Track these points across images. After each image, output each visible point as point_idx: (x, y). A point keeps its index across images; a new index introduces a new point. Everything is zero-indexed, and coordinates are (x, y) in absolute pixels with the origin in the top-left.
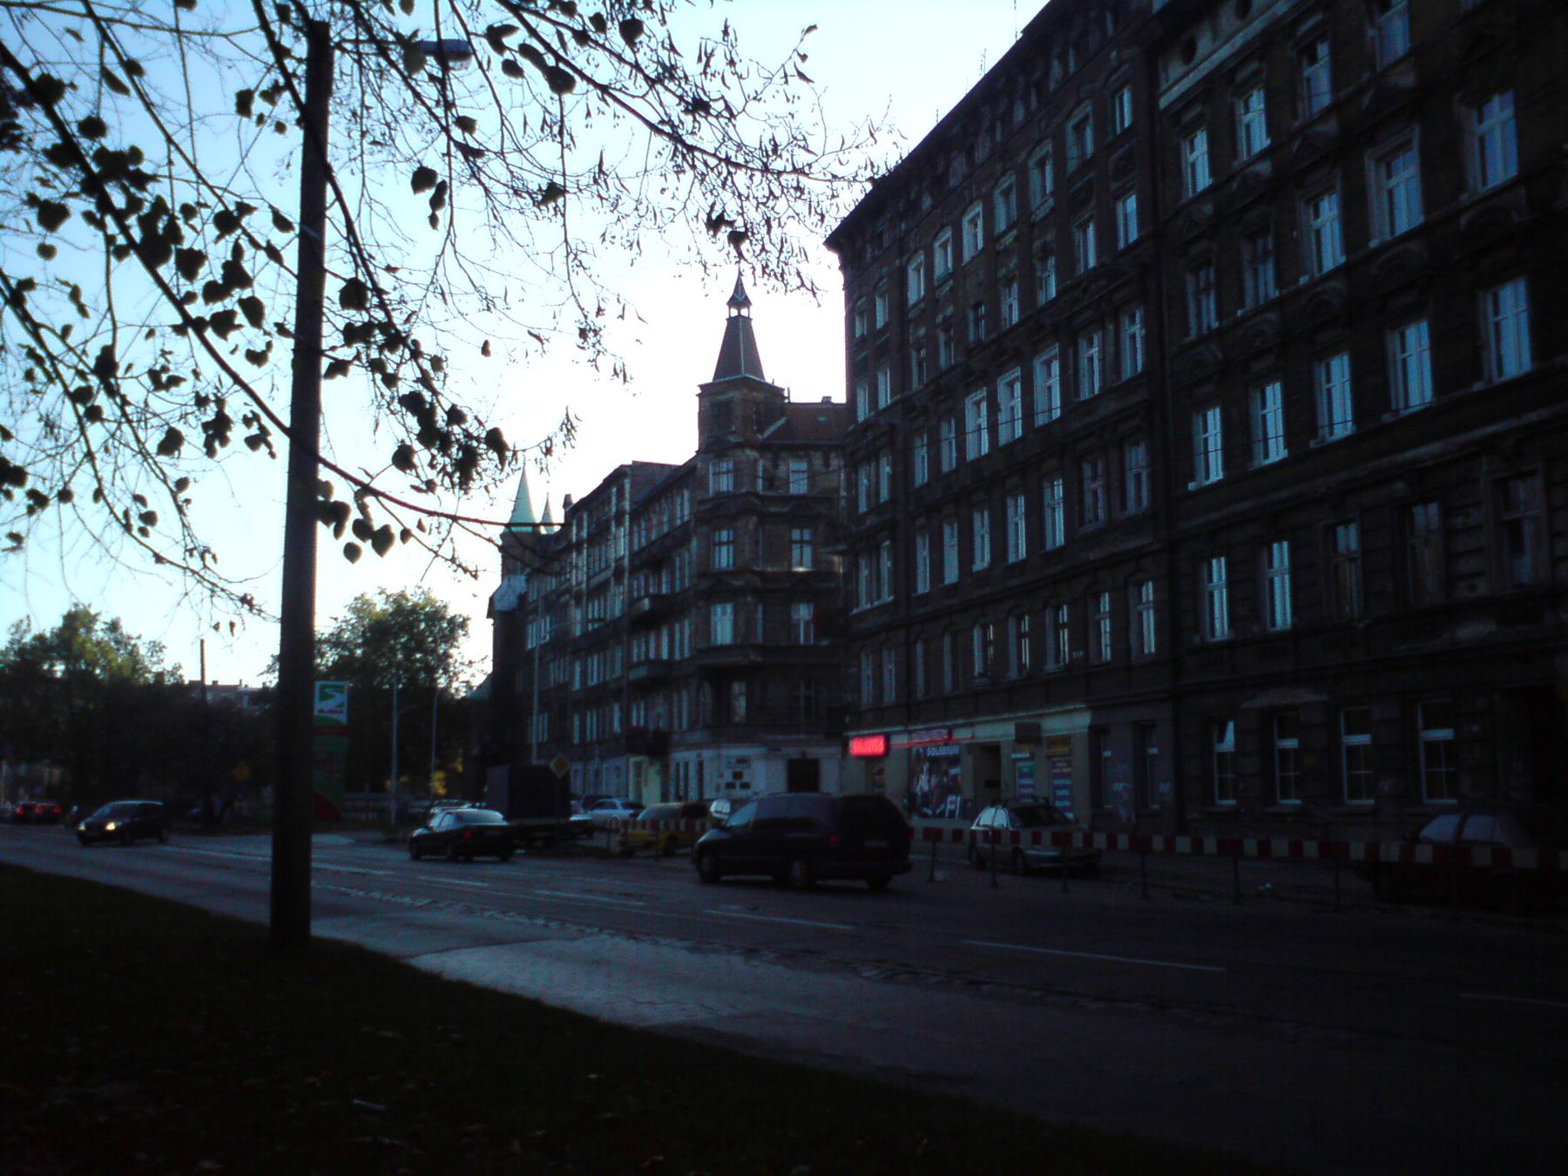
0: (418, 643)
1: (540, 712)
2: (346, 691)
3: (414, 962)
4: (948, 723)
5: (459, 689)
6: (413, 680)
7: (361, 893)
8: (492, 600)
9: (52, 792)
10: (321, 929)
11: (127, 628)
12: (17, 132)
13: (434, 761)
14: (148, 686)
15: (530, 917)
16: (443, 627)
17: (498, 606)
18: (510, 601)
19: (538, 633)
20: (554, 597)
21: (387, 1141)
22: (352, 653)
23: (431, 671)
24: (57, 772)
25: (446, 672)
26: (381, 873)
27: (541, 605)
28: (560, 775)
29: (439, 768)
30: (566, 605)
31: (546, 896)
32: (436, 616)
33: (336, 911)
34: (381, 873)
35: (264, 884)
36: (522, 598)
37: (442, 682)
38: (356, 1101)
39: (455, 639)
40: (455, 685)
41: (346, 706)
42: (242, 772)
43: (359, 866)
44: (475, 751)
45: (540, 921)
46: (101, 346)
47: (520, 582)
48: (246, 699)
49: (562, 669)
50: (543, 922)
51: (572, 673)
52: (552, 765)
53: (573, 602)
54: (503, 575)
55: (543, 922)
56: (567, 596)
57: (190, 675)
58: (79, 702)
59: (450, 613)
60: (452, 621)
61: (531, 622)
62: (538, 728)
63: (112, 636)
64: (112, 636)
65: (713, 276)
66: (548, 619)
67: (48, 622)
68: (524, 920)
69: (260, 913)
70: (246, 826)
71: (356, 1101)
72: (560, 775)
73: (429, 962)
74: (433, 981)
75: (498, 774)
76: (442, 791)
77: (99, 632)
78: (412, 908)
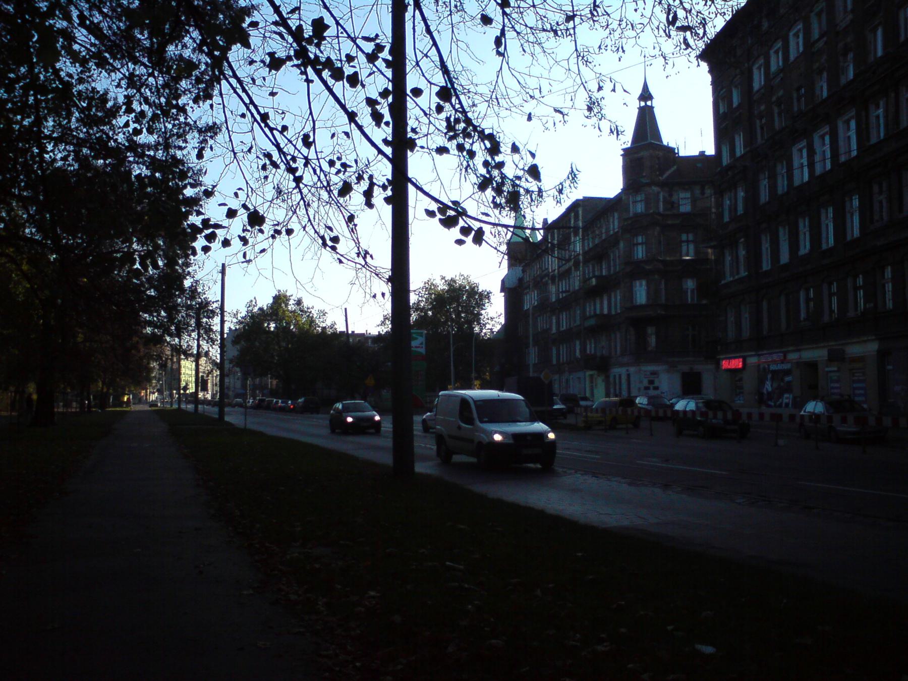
2: (424, 336)
8: (503, 282)
13: (473, 375)
17: (507, 285)
19: (530, 300)
21: (466, 586)
23: (470, 323)
25: (479, 324)
28: (547, 382)
29: (476, 379)
30: (546, 284)
36: (520, 280)
38: (448, 563)
44: (497, 369)
47: (519, 270)
52: (542, 376)
53: (550, 282)
58: (284, 344)
60: (481, 295)
61: (526, 294)
62: (533, 356)
67: (265, 301)
71: (448, 563)
77: (292, 307)
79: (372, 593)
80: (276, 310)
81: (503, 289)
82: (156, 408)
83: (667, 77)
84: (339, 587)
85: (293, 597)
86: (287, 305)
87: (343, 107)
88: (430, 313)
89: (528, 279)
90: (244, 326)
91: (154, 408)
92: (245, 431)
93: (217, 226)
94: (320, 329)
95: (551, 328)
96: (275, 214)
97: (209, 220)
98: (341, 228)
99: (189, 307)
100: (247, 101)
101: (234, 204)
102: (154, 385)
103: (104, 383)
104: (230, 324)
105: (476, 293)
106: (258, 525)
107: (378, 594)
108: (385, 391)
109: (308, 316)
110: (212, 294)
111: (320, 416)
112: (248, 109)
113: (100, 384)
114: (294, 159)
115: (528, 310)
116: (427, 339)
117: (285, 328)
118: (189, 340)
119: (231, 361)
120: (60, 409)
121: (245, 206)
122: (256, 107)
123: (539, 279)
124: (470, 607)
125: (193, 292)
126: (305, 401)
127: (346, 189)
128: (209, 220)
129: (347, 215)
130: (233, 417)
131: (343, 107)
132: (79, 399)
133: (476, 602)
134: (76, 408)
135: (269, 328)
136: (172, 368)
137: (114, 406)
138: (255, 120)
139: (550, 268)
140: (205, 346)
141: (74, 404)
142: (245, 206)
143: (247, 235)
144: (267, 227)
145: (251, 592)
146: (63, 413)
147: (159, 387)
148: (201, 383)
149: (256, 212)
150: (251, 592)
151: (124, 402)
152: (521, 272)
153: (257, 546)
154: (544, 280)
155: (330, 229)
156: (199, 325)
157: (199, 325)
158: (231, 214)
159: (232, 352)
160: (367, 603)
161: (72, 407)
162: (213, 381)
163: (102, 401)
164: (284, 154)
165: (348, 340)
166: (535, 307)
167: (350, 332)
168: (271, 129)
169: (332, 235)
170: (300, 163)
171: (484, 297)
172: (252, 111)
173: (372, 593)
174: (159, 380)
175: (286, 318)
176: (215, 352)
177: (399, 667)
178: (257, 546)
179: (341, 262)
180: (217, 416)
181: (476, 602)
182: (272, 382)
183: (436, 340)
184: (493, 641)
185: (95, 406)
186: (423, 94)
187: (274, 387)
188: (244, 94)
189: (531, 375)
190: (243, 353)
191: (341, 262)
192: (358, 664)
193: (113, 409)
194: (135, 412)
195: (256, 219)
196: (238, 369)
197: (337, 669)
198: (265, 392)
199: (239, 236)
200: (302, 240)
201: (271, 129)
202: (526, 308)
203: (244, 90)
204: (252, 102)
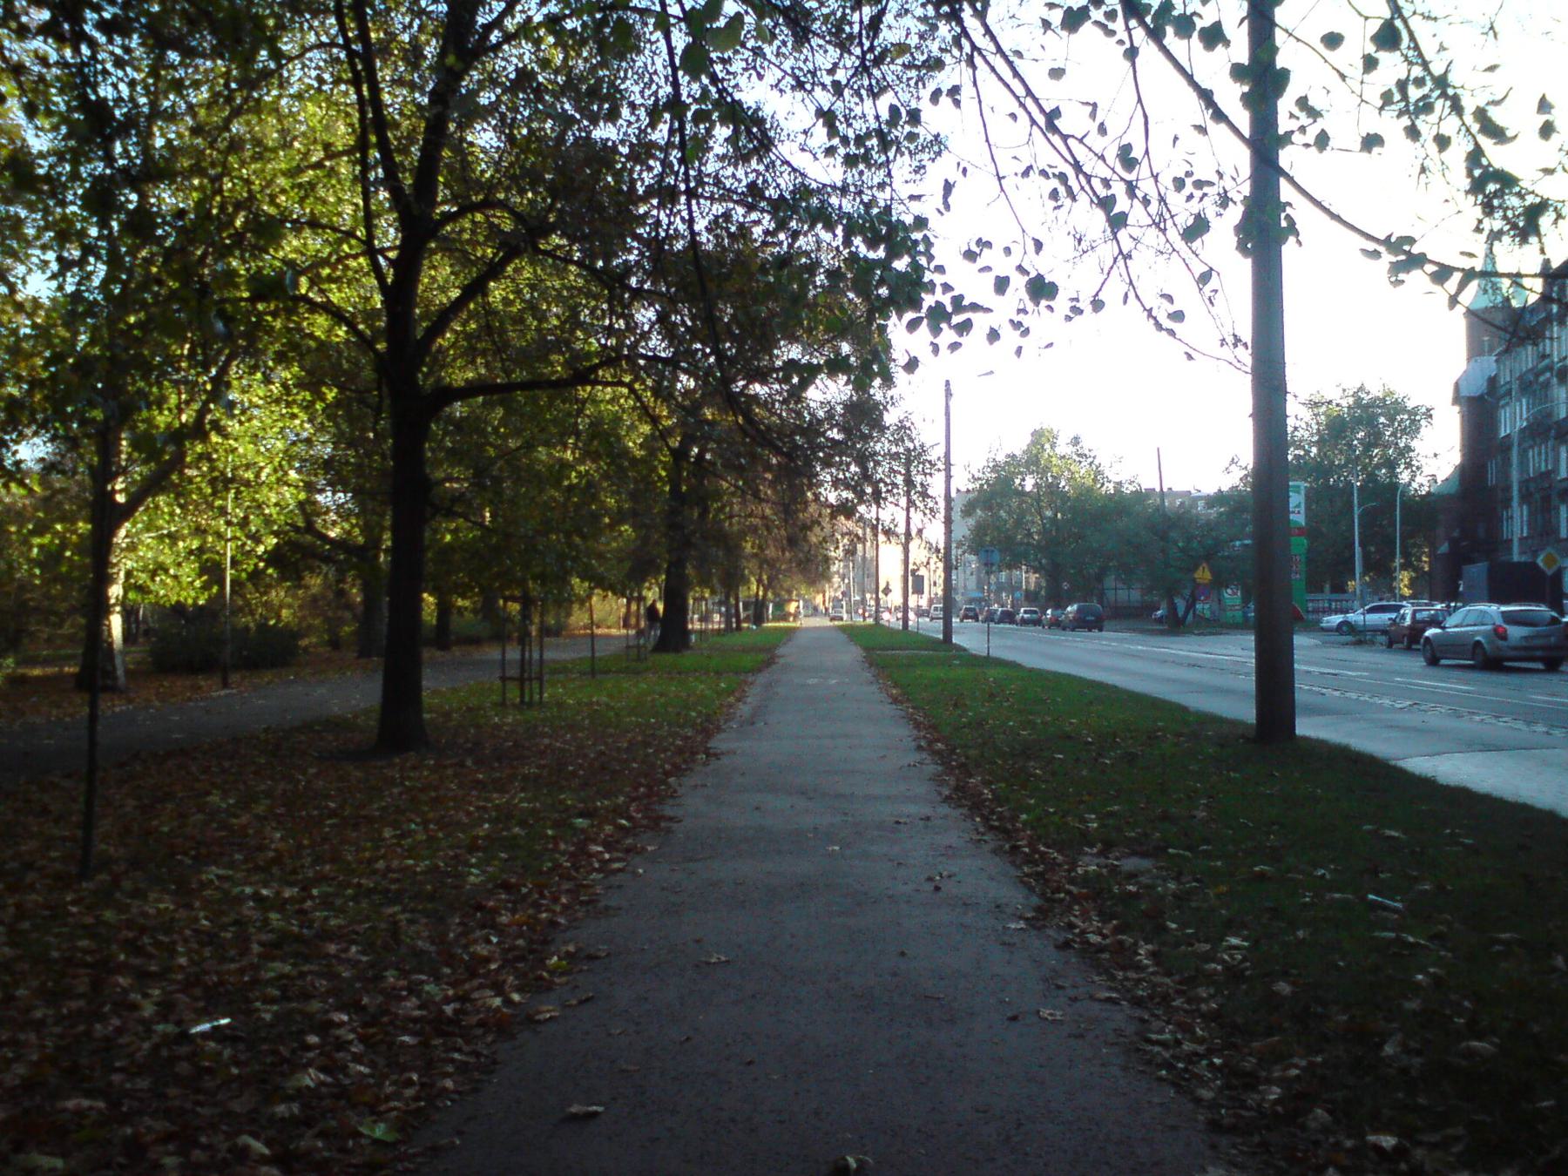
0: (1375, 439)
1: (1521, 505)
2: (1303, 492)
3: (1401, 764)
4: (309, 538)
5: (1421, 484)
6: (1372, 477)
7: (1337, 694)
8: (1457, 386)
9: (1031, 597)
10: (1305, 727)
11: (1086, 444)
12: (610, 144)
13: (1398, 561)
14: (1110, 497)
15: (1529, 723)
16: (1414, 420)
17: (1465, 393)
18: (1478, 387)
19: (1513, 419)
20: (1531, 378)
21: (1411, 939)
22: (1308, 452)
23: (1391, 465)
24: (1033, 577)
25: (1409, 465)
26: (1354, 674)
27: (1515, 386)
28: (1549, 573)
29: (1404, 567)
30: (1547, 385)
31: (1544, 702)
32: (1393, 408)
33: (1315, 711)
34: (1354, 674)
35: (1249, 683)
36: (1492, 381)
37: (1404, 477)
38: (1371, 897)
39: (1418, 430)
40: (1419, 479)
41: (1303, 506)
42: (1204, 575)
43: (1328, 666)
44: (1444, 548)
45: (1540, 728)
46: (1231, 81)
47: (1489, 364)
48: (1201, 504)
49: (1543, 457)
50: (1544, 729)
51: (1557, 461)
52: (1540, 561)
53: (1555, 380)
54: (1469, 360)
55: (1544, 729)
56: (1548, 375)
57: (1149, 482)
58: (1049, 513)
59: (1410, 405)
60: (1413, 412)
61: (1503, 407)
62: (1517, 522)
63: (1074, 449)
64: (1074, 449)
65: (1487, 17)
66: (1524, 401)
67: (1018, 444)
68: (1520, 725)
69: (1247, 712)
70: (1216, 626)
71: (1371, 897)
72: (1549, 573)
73: (1419, 765)
74: (1427, 787)
75: (1476, 571)
76: (1407, 592)
77: (1063, 448)
78: (1393, 710)
79: (1234, 941)
80: (1036, 456)
81: (1457, 399)
82: (841, 623)
83: (1492, 68)
84: (1174, 926)
85: (1094, 938)
86: (1053, 446)
87: (1190, 79)
88: (1314, 450)
89: (1508, 379)
90: (982, 485)
91: (837, 623)
92: (988, 661)
93: (975, 307)
94: (1111, 486)
95: (1556, 470)
96: (1075, 280)
97: (961, 297)
98: (1188, 297)
99: (895, 457)
100: (1021, 91)
101: (1005, 267)
102: (836, 585)
103: (759, 581)
104: (962, 482)
105: (1404, 410)
106: (1024, 817)
107: (1246, 944)
108: (1229, 591)
109: (1091, 464)
110: (928, 435)
111: (1104, 634)
112: (1022, 105)
113: (754, 587)
114: (1106, 183)
115: (1508, 436)
116: (1307, 497)
117: (1049, 486)
118: (891, 513)
119: (960, 544)
120: (695, 625)
121: (1020, 268)
122: (1036, 100)
123: (1531, 378)
124: (1420, 977)
125: (902, 428)
126: (1079, 610)
127: (1198, 228)
128: (961, 297)
129: (1199, 269)
130: (969, 637)
131: (1190, 79)
132: (723, 609)
133: (1432, 970)
134: (720, 623)
135: (1023, 486)
136: (864, 557)
137: (776, 619)
138: (1033, 122)
139: (1556, 353)
140: (917, 518)
141: (717, 617)
142: (1020, 268)
143: (1026, 321)
144: (1061, 303)
145: (1022, 924)
146: (701, 632)
147: (843, 588)
148: (913, 581)
149: (1040, 277)
150: (1022, 924)
151: (790, 614)
152: (1494, 365)
153: (1027, 850)
154: (1542, 379)
155: (1169, 298)
156: (909, 482)
157: (909, 482)
158: (1002, 285)
159: (962, 529)
160: (1226, 957)
161: (713, 622)
162: (934, 575)
163: (758, 611)
164: (1088, 178)
165: (1163, 501)
166: (1522, 430)
167: (1165, 490)
168: (1065, 138)
169: (1172, 309)
170: (1119, 189)
171: (1414, 420)
172: (1030, 109)
173: (1234, 941)
174: (843, 578)
175: (1054, 469)
176: (935, 532)
177: (1294, 1072)
178: (1027, 850)
179: (1190, 357)
180: (941, 636)
181: (1432, 970)
182: (1028, 579)
183: (1329, 500)
184: (1475, 1044)
185: (747, 619)
186: (1345, 42)
187: (1032, 587)
188: (1016, 80)
189: (1516, 558)
190: (980, 531)
191: (1190, 357)
192: (1217, 1061)
193: (777, 624)
194: (808, 629)
195: (1041, 289)
196: (973, 557)
197: (1181, 1065)
198: (1018, 594)
199: (1012, 321)
200: (1122, 318)
201: (1065, 138)
202: (1503, 434)
203: (1016, 74)
204: (1029, 92)
